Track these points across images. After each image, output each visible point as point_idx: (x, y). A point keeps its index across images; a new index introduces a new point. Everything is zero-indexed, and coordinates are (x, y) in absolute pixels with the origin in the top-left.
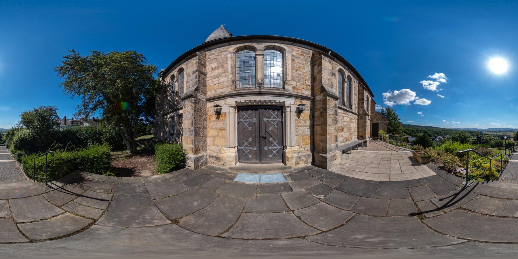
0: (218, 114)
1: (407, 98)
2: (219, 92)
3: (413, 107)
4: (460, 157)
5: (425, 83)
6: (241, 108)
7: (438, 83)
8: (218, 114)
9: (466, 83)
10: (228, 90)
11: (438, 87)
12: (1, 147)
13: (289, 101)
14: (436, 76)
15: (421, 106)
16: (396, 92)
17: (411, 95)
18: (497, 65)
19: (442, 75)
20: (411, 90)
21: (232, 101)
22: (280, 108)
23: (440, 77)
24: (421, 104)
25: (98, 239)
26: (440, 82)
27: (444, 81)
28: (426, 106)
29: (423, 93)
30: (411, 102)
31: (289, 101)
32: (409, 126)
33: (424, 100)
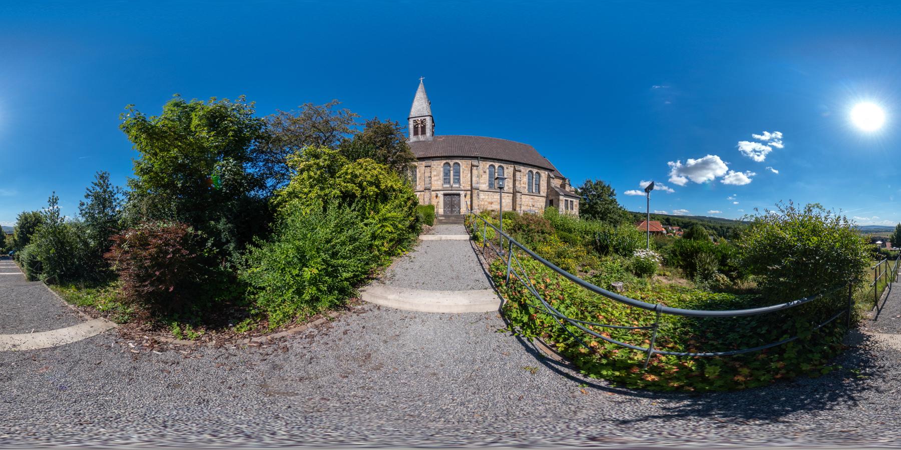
0: (437, 196)
1: (713, 170)
2: (437, 188)
3: (718, 187)
4: (777, 322)
5: (746, 146)
6: (445, 195)
7: (770, 149)
8: (437, 196)
9: (815, 145)
10: (440, 188)
11: (769, 156)
12: (3, 262)
13: (461, 192)
14: (767, 136)
15: (735, 186)
16: (691, 162)
17: (719, 167)
18: (865, 115)
19: (779, 135)
20: (722, 159)
21: (442, 192)
22: (459, 195)
23: (774, 139)
24: (735, 183)
25: (376, 279)
26: (773, 147)
27: (779, 145)
28: (741, 186)
29: (738, 162)
30: (718, 179)
31: (461, 192)
32: (711, 219)
33: (740, 174)
